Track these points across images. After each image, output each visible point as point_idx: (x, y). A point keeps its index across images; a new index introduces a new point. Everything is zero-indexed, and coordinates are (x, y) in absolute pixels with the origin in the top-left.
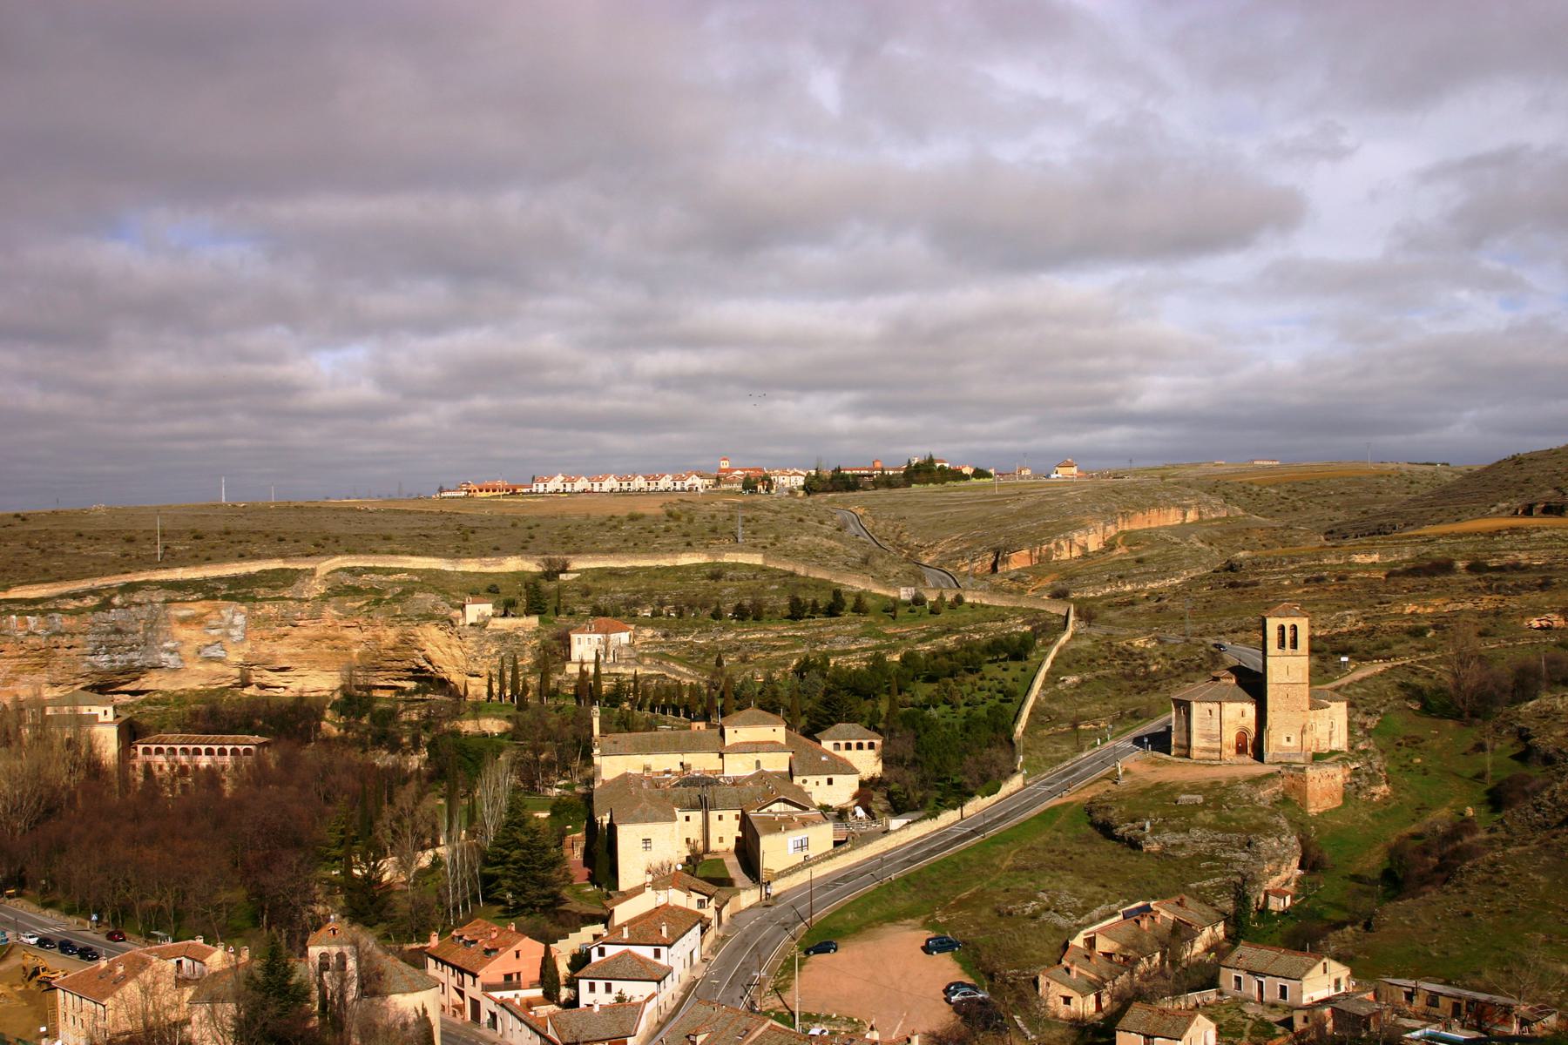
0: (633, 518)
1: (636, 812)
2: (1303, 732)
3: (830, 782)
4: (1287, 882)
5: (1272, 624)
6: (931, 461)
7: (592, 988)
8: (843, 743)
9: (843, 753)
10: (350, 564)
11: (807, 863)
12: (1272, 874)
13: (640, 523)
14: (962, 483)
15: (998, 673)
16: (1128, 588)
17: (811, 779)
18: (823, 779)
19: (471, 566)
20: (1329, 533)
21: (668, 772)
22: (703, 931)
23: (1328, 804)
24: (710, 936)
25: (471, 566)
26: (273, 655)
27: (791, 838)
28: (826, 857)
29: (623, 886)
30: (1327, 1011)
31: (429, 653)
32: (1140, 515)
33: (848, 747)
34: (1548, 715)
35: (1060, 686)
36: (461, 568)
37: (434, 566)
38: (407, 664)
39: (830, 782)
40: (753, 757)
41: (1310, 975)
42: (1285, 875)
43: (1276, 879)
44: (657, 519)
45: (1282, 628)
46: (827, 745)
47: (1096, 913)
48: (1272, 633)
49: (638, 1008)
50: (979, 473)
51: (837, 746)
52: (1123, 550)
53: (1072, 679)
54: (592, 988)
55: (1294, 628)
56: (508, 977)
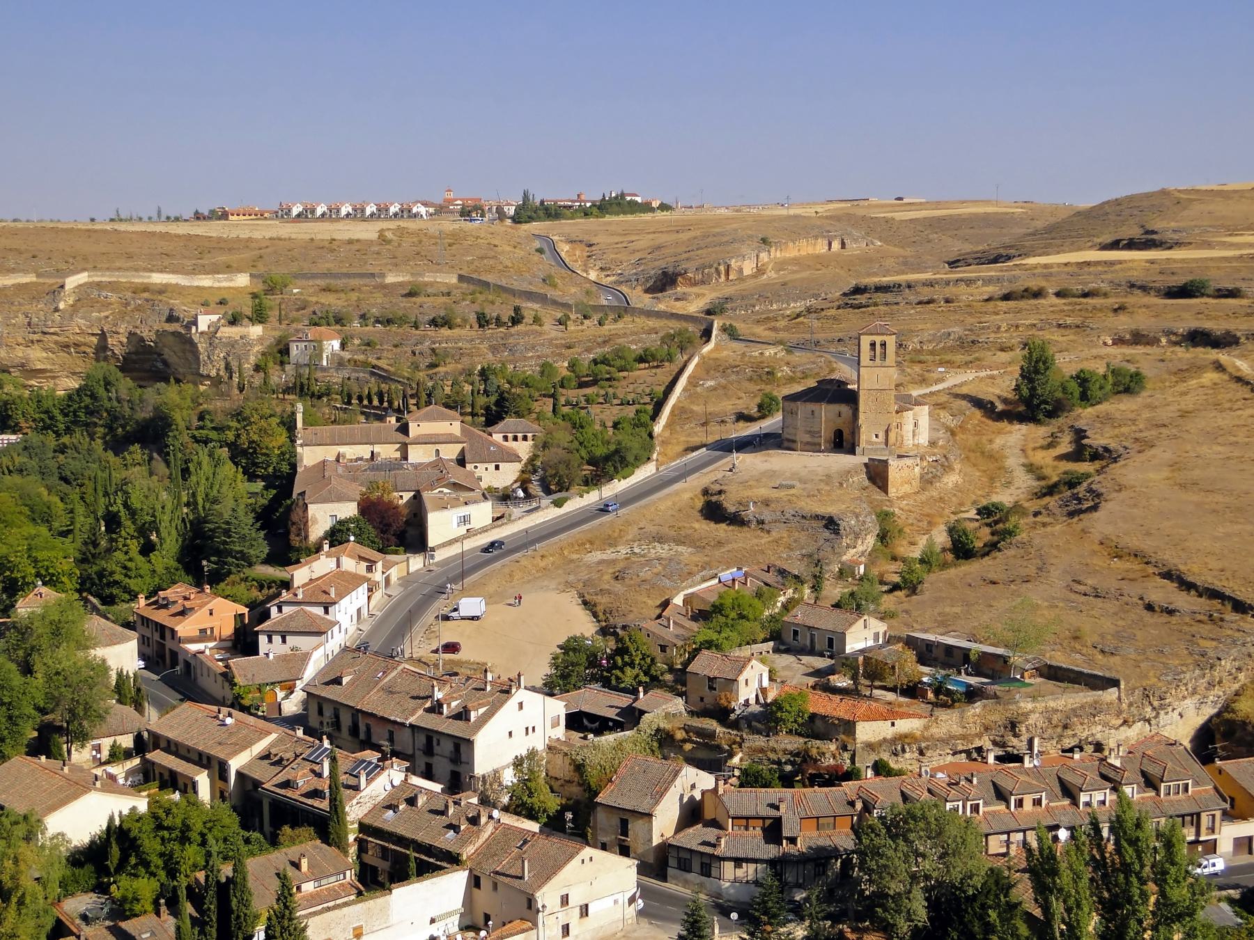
0: (350, 242)
1: (324, 492)
2: (887, 432)
3: (497, 468)
4: (863, 553)
5: (866, 341)
6: (623, 195)
7: (270, 641)
8: (510, 436)
9: (511, 444)
10: (97, 279)
11: (470, 533)
12: (848, 547)
13: (356, 247)
14: (648, 216)
15: (645, 379)
16: (775, 306)
17: (481, 466)
18: (492, 466)
19: (205, 281)
20: (950, 263)
21: (361, 459)
22: (370, 590)
23: (907, 489)
24: (378, 595)
25: (205, 281)
26: (28, 360)
27: (453, 515)
28: (484, 530)
29: (431, 544)
30: (861, 659)
31: (166, 357)
32: (791, 244)
33: (515, 439)
34: (1107, 419)
35: (698, 389)
36: (196, 284)
37: (174, 281)
38: (147, 366)
39: (497, 468)
40: (434, 447)
41: (853, 629)
42: (860, 548)
43: (852, 551)
44: (370, 243)
45: (873, 345)
46: (497, 437)
47: (698, 577)
48: (865, 346)
49: (305, 657)
50: (664, 207)
51: (506, 438)
52: (773, 275)
53: (710, 383)
54: (270, 641)
55: (884, 345)
56: (203, 631)
